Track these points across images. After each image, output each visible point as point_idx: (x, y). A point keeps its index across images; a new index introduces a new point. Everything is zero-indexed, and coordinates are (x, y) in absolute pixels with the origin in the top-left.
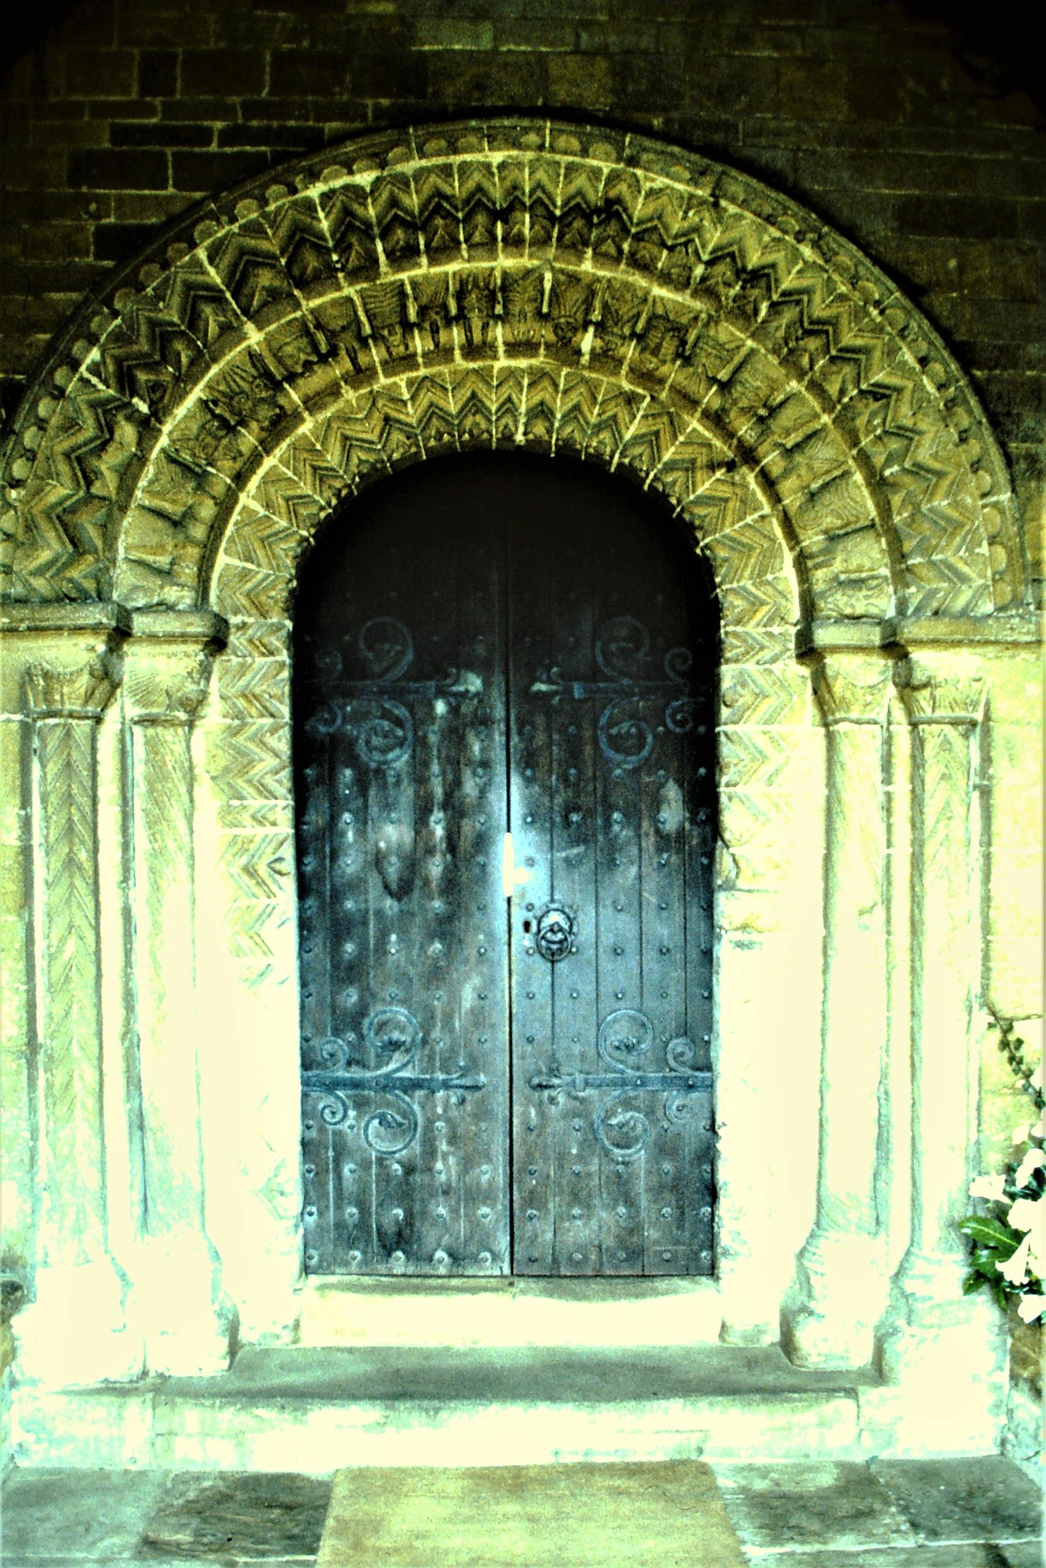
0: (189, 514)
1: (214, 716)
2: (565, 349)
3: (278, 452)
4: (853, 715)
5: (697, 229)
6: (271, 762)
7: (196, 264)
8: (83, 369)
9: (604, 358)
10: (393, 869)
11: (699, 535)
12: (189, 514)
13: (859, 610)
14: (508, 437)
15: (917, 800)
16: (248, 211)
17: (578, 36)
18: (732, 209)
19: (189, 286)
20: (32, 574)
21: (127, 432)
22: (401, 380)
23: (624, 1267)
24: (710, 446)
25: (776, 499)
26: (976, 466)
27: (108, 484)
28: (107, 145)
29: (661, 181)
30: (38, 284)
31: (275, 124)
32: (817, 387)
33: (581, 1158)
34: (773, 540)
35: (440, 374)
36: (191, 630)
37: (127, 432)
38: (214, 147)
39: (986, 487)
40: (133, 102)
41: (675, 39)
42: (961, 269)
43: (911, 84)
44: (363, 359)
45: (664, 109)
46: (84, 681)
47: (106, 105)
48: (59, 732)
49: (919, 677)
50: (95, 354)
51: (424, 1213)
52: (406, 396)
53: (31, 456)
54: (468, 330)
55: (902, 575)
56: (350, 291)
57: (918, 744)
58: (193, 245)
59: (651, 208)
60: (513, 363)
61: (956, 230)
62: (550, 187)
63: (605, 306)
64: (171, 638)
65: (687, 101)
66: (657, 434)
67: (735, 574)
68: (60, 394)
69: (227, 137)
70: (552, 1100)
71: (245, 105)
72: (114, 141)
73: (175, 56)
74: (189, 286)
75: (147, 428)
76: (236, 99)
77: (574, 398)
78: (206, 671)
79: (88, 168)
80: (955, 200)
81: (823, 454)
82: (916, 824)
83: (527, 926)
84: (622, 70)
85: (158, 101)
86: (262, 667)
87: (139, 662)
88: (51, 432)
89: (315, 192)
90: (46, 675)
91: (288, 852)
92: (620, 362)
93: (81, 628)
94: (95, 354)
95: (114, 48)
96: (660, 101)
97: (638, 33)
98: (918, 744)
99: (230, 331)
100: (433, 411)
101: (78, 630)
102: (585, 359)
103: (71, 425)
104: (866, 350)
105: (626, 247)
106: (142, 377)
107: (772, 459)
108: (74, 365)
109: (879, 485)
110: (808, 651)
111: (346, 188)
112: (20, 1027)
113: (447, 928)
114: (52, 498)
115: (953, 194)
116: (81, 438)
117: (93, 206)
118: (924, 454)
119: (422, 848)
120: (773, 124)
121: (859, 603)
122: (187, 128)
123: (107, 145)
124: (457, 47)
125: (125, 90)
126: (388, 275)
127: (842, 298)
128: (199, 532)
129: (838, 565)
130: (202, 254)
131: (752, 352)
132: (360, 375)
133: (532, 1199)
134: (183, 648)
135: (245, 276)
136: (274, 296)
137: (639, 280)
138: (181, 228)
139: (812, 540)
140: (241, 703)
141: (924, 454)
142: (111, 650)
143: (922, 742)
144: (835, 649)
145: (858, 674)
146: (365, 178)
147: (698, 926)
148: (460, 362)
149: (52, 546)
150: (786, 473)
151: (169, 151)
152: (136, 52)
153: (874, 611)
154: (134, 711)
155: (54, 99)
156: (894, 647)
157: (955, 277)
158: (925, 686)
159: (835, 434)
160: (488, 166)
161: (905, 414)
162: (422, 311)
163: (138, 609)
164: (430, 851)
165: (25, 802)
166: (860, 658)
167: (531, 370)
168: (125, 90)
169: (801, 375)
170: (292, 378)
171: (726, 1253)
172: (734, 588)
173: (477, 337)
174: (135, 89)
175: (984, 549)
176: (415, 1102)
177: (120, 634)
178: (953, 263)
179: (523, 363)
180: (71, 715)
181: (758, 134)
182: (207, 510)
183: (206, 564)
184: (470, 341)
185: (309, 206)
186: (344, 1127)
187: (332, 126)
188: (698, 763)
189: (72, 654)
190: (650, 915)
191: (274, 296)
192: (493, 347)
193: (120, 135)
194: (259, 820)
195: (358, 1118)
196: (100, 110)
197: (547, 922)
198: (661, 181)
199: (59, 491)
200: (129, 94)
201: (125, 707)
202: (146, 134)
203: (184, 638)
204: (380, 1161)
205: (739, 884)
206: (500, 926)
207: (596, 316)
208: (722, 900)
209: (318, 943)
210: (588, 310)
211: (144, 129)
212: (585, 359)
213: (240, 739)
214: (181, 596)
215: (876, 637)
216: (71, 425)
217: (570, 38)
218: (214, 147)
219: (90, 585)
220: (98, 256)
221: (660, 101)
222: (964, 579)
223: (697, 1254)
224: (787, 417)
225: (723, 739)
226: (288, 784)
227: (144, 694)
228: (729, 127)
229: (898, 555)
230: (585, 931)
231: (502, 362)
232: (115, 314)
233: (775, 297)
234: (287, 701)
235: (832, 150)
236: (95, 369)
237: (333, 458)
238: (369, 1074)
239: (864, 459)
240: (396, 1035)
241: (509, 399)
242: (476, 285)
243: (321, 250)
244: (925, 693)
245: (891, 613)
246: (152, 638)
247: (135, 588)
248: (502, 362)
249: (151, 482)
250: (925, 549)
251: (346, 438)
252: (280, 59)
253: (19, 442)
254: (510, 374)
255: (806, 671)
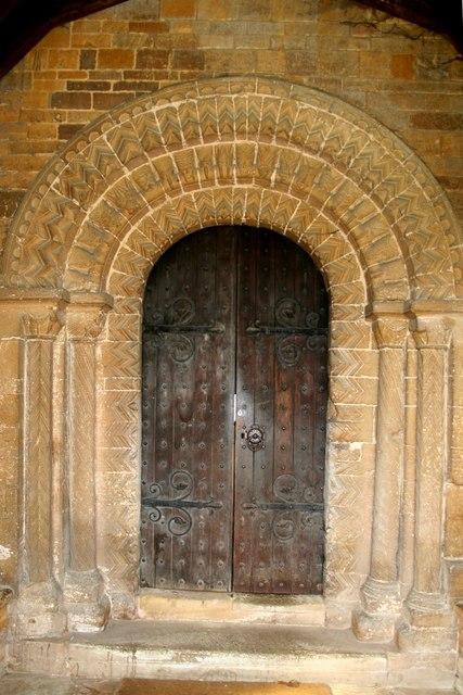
0: (98, 251)
1: (105, 338)
2: (264, 180)
3: (137, 224)
4: (391, 344)
5: (322, 126)
6: (131, 360)
7: (102, 141)
8: (51, 186)
9: (281, 184)
10: (184, 409)
11: (322, 262)
12: (98, 251)
13: (394, 297)
14: (239, 219)
15: (419, 382)
16: (125, 119)
17: (271, 43)
18: (338, 117)
19: (98, 151)
20: (27, 275)
21: (70, 213)
22: (192, 193)
23: (281, 590)
24: (327, 224)
25: (357, 247)
26: (448, 232)
27: (60, 236)
28: (66, 90)
29: (306, 106)
30: (34, 150)
31: (138, 81)
32: (375, 197)
33: (264, 540)
34: (355, 265)
35: (209, 191)
36: (97, 301)
37: (70, 213)
38: (111, 91)
39: (452, 241)
40: (76, 73)
41: (313, 41)
42: (441, 143)
43: (419, 62)
44: (210, 175)
45: (309, 74)
46: (47, 323)
47: (64, 73)
48: (36, 346)
49: (421, 328)
50: (57, 180)
51: (194, 563)
52: (194, 200)
53: (28, 224)
54: (220, 170)
55: (412, 282)
56: (171, 154)
57: (420, 357)
58: (100, 133)
59: (301, 117)
60: (241, 186)
61: (439, 127)
62: (257, 109)
63: (281, 162)
64: (86, 305)
65: (318, 70)
66: (304, 218)
67: (338, 280)
68: (40, 197)
69: (107, 86)
70: (252, 514)
71: (125, 73)
72: (68, 88)
73: (95, 52)
74: (98, 151)
75: (79, 215)
76: (121, 71)
77: (268, 201)
78: (102, 319)
79: (58, 100)
80: (437, 114)
81: (378, 227)
82: (419, 394)
83: (243, 435)
84: (290, 58)
85: (87, 71)
86: (129, 317)
87: (72, 315)
88: (36, 214)
89: (154, 110)
90: (31, 320)
91: (138, 401)
92: (288, 185)
93: (48, 299)
94: (57, 180)
95: (69, 48)
96: (307, 70)
97: (298, 41)
98: (420, 357)
99: (118, 172)
100: (204, 208)
101: (45, 300)
102: (273, 184)
103: (45, 210)
104: (398, 180)
105: (291, 134)
106: (77, 189)
107: (355, 229)
108: (48, 185)
109: (403, 242)
110: (370, 314)
111: (167, 108)
112: (340, 328)
113: (205, 436)
114: (37, 242)
115: (437, 111)
116: (50, 216)
117: (58, 117)
118: (424, 227)
119: (197, 397)
120: (357, 80)
121: (394, 294)
122: (100, 83)
123: (66, 90)
124: (218, 47)
125: (74, 66)
126: (186, 148)
127: (387, 157)
128: (101, 259)
129: (384, 277)
130: (105, 137)
131: (347, 181)
132: (174, 191)
133: (242, 557)
134: (92, 309)
135: (123, 146)
136: (135, 157)
137: (296, 150)
138: (96, 128)
139: (374, 265)
140: (119, 334)
141: (424, 227)
142: (59, 309)
143: (422, 357)
144: (383, 314)
145: (394, 325)
146: (176, 105)
147: (318, 437)
148: (218, 186)
149: (35, 264)
150: (362, 235)
151: (92, 92)
152: (79, 50)
153: (401, 297)
154: (70, 336)
155: (43, 70)
156: (409, 313)
157: (439, 147)
158: (424, 331)
159: (383, 218)
160: (230, 99)
161: (416, 208)
162: (201, 164)
163: (74, 292)
164: (200, 401)
165: (20, 376)
166: (393, 319)
167: (249, 190)
168: (74, 66)
169: (368, 191)
170: (143, 191)
171: (328, 586)
172: (337, 287)
173: (225, 174)
174: (78, 65)
175: (451, 269)
176: (191, 511)
177: (64, 302)
178: (438, 142)
179: (245, 186)
180: (41, 338)
181: (351, 85)
182: (105, 249)
183: (104, 272)
184: (221, 177)
185: (151, 116)
186: (159, 522)
187: (162, 82)
188: (321, 361)
189: (41, 311)
190: (298, 434)
191: (135, 157)
192: (178, 187)
193: (71, 86)
194: (125, 386)
195: (166, 519)
196: (62, 75)
197: (252, 434)
198: (306, 106)
199: (40, 240)
200: (131, 67)
201: (65, 335)
202: (82, 86)
203: (93, 304)
204: (175, 539)
205: (339, 419)
206: (231, 435)
207: (277, 165)
208: (330, 426)
209: (149, 441)
210: (274, 163)
211: (81, 83)
212: (273, 184)
213: (118, 351)
214: (92, 286)
215: (400, 308)
216: (45, 210)
217: (267, 42)
218: (111, 91)
219: (51, 281)
220: (60, 138)
221: (307, 70)
222: (441, 283)
223: (315, 586)
224: (363, 210)
225: (332, 354)
226: (139, 370)
227: (75, 329)
228: (337, 82)
229: (411, 272)
230: (269, 438)
231: (236, 186)
232: (67, 162)
233: (357, 157)
234: (138, 333)
235: (383, 92)
236: (57, 187)
237: (161, 227)
238: (171, 499)
239: (397, 229)
240: (184, 483)
241: (239, 202)
242: (225, 150)
243: (157, 137)
244: (424, 334)
245: (409, 298)
246: (79, 304)
247: (73, 282)
248: (236, 186)
249: (81, 236)
250: (424, 270)
251: (167, 219)
252: (140, 54)
253: (23, 218)
254: (239, 191)
255: (369, 324)
